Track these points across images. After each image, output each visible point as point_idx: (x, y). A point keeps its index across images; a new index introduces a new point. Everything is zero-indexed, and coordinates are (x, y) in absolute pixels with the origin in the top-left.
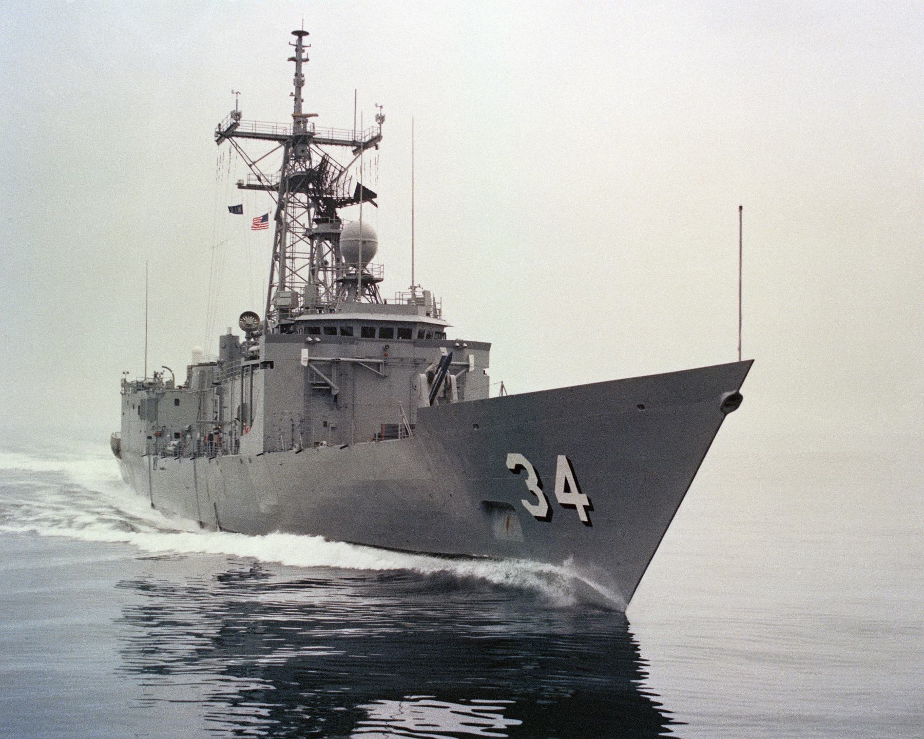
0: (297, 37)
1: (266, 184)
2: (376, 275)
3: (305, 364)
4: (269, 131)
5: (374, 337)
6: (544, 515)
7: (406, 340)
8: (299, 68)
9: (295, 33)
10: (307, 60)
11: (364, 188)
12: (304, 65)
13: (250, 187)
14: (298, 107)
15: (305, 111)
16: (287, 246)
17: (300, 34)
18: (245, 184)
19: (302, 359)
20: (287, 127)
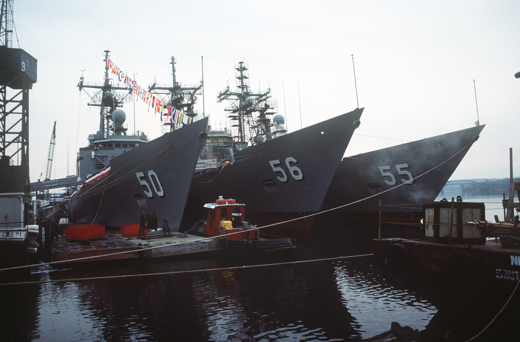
0: (106, 53)
1: (97, 104)
2: (210, 125)
3: (93, 157)
4: (94, 85)
6: (162, 195)
8: (173, 66)
9: (105, 51)
10: (176, 63)
12: (175, 64)
13: (92, 105)
17: (107, 52)
18: (90, 104)
19: (92, 155)
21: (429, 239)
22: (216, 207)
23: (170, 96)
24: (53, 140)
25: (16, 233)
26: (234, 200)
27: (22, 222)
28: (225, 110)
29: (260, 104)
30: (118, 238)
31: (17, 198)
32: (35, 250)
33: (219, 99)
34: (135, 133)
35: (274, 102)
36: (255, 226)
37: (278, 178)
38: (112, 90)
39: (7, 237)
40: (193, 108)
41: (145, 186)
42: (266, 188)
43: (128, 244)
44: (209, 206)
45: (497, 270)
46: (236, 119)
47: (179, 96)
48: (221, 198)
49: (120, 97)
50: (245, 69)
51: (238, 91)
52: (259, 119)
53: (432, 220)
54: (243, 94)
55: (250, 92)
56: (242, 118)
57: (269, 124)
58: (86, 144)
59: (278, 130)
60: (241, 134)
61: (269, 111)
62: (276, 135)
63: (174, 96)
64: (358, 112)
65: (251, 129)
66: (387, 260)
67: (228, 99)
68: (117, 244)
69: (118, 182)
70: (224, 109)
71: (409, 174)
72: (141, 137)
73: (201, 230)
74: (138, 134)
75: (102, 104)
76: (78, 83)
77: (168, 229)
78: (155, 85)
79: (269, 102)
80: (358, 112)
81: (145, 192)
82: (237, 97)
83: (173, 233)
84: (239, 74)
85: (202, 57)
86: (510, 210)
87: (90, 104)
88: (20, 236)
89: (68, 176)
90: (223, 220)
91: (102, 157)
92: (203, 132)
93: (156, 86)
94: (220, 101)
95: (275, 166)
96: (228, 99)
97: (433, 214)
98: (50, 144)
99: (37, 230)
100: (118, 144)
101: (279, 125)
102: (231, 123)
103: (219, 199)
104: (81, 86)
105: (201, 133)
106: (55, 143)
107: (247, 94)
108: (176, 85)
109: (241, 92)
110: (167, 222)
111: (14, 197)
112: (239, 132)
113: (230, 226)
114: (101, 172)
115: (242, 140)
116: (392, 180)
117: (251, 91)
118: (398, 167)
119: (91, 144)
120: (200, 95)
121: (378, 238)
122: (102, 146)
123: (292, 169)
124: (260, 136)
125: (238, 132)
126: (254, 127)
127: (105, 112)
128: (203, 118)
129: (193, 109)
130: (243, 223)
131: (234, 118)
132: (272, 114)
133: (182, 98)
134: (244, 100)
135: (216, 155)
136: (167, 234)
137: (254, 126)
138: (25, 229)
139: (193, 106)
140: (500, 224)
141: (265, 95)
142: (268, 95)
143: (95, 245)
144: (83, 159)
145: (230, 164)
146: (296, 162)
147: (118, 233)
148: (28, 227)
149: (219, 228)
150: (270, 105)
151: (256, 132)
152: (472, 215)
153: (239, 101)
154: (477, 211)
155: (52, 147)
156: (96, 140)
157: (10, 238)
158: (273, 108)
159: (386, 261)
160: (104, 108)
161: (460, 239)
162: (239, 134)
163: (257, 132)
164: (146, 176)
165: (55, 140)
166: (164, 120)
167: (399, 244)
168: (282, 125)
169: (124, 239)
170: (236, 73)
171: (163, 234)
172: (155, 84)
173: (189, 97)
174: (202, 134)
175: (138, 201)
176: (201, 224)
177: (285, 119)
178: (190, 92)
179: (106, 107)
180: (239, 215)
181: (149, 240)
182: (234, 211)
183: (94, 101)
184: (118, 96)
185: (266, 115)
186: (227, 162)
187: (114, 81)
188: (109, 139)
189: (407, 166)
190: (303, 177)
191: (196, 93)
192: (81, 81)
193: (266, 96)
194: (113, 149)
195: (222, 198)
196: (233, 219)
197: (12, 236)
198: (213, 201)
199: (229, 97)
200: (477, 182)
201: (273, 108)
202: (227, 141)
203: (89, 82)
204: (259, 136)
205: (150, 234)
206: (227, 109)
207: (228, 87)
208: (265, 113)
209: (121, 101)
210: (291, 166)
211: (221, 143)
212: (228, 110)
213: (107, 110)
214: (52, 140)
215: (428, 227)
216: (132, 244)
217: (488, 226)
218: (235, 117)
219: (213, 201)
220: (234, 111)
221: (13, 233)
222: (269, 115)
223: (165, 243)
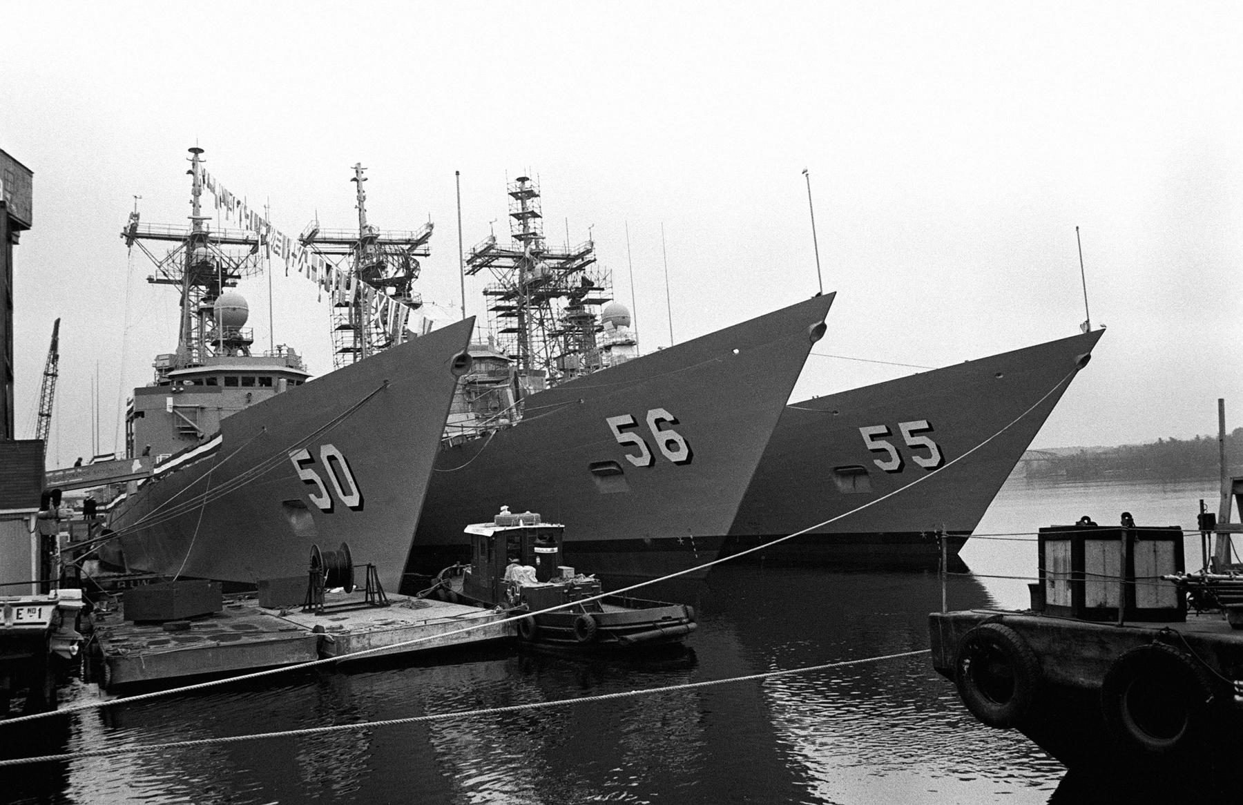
1: (171, 278)
3: (171, 411)
5: (237, 386)
6: (357, 504)
7: (267, 387)
11: (967, 538)
13: (159, 281)
14: (196, 211)
15: (202, 215)
16: (193, 327)
17: (196, 151)
20: (186, 229)
21: (1057, 610)
22: (495, 532)
23: (352, 259)
24: (51, 365)
25: (29, 610)
26: (537, 514)
27: (34, 582)
28: (485, 293)
29: (570, 278)
30: (254, 612)
31: (20, 521)
32: (74, 650)
33: (471, 265)
34: (272, 350)
35: (603, 273)
36: (591, 576)
37: (629, 457)
38: (209, 245)
39: (7, 621)
40: (410, 288)
41: (312, 482)
42: (598, 481)
43: (290, 628)
44: (477, 530)
45: (1236, 682)
46: (512, 315)
47: (375, 260)
48: (505, 512)
49: (231, 263)
50: (531, 194)
51: (516, 246)
52: (568, 315)
53: (1065, 569)
54: (528, 255)
55: (544, 250)
56: (525, 311)
57: (594, 326)
58: (149, 378)
59: (614, 340)
60: (523, 351)
61: (592, 295)
62: (610, 354)
63: (362, 260)
64: (823, 302)
65: (547, 338)
66: (968, 661)
67: (492, 266)
68: (260, 629)
69: (254, 476)
70: (483, 290)
71: (931, 445)
72: (287, 359)
73: (457, 587)
74: (278, 352)
75: (184, 277)
76: (125, 228)
77: (377, 586)
78: (317, 233)
79: (591, 272)
80: (823, 302)
81: (312, 496)
82: (514, 261)
83: (389, 596)
84: (517, 206)
85: (457, 173)
86: (1223, 540)
87: (155, 280)
88: (40, 617)
89: (96, 455)
90: (512, 565)
91: (194, 411)
92: (462, 352)
93: (319, 236)
94: (472, 273)
95: (621, 428)
96: (492, 266)
97: (1069, 553)
98: (43, 375)
99: (78, 600)
100: (232, 379)
101: (616, 328)
102: (500, 325)
103: (501, 513)
104: (132, 235)
105: (457, 355)
106: (58, 373)
107: (539, 255)
108: (368, 232)
109: (522, 250)
110: (375, 571)
111: (12, 520)
112: (519, 345)
113: (531, 577)
114: (197, 448)
115: (526, 364)
116: (890, 460)
117: (546, 248)
118: (905, 427)
119: (161, 377)
120: (424, 257)
121: (941, 610)
122: (192, 383)
123: (661, 438)
124: (572, 355)
125: (516, 346)
126: (554, 335)
127: (193, 299)
128: (462, 319)
129: (411, 292)
130: (562, 570)
131: (508, 312)
132: (600, 302)
133: (381, 266)
134: (531, 269)
135: (469, 403)
136: (374, 601)
137: (556, 331)
138: (49, 599)
139: (410, 285)
140: (1231, 577)
141: (581, 256)
142: (589, 257)
143: (205, 633)
144: (143, 417)
145: (512, 425)
146: (673, 419)
147: (249, 598)
148: (56, 595)
149: (504, 582)
150: (593, 280)
151: (559, 346)
152: (1155, 554)
153: (517, 271)
154: (1168, 546)
155: (49, 383)
156: (176, 368)
157: (15, 624)
158: (601, 287)
159: (967, 664)
160: (189, 290)
161: (1130, 610)
162: (518, 351)
163: (563, 345)
164: (315, 457)
165: (56, 366)
166: (339, 317)
167: (998, 625)
168: (624, 329)
169: (271, 615)
170: (511, 203)
171: (364, 600)
172: (315, 232)
173: (401, 261)
174: (459, 359)
175: (294, 520)
176: (454, 574)
177: (632, 315)
178: (402, 249)
179: (196, 286)
180: (553, 550)
181: (335, 616)
182: (538, 541)
183: (164, 272)
184: (227, 260)
185: (586, 306)
186: (501, 421)
187: (219, 223)
188: (208, 366)
189: (926, 426)
190: (690, 455)
191: (416, 252)
192: (132, 221)
193: (583, 260)
194: (219, 391)
195: (508, 510)
196: (538, 560)
197: (18, 618)
198: (486, 517)
199: (495, 263)
200: (1060, 454)
201: (603, 289)
202: (496, 369)
203: (151, 225)
204: (568, 356)
205: (331, 601)
206: (489, 290)
207: (494, 239)
208: (582, 300)
209: (233, 272)
210: (660, 430)
211: (481, 372)
212: (491, 293)
213: (198, 293)
214: (48, 365)
215: (1053, 583)
216: (299, 628)
217: (1207, 583)
218: (510, 308)
219: (487, 518)
220: (507, 297)
221: (20, 612)
222: (592, 306)
223: (380, 623)
